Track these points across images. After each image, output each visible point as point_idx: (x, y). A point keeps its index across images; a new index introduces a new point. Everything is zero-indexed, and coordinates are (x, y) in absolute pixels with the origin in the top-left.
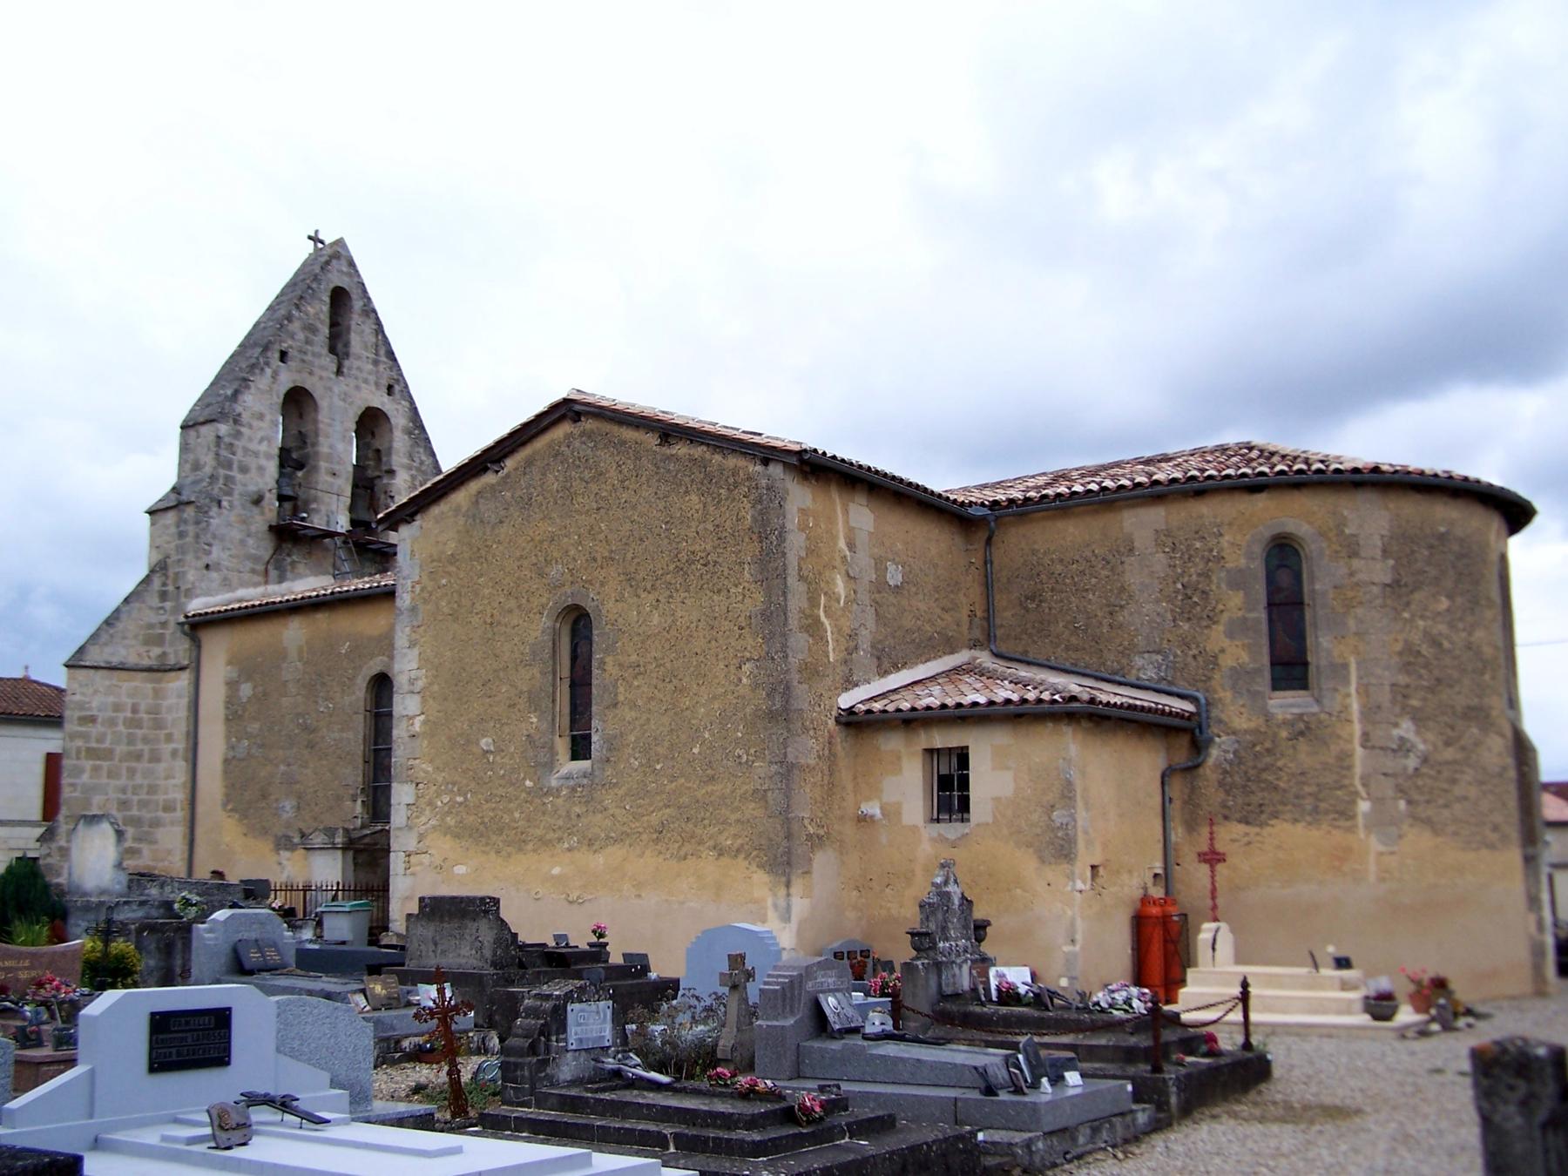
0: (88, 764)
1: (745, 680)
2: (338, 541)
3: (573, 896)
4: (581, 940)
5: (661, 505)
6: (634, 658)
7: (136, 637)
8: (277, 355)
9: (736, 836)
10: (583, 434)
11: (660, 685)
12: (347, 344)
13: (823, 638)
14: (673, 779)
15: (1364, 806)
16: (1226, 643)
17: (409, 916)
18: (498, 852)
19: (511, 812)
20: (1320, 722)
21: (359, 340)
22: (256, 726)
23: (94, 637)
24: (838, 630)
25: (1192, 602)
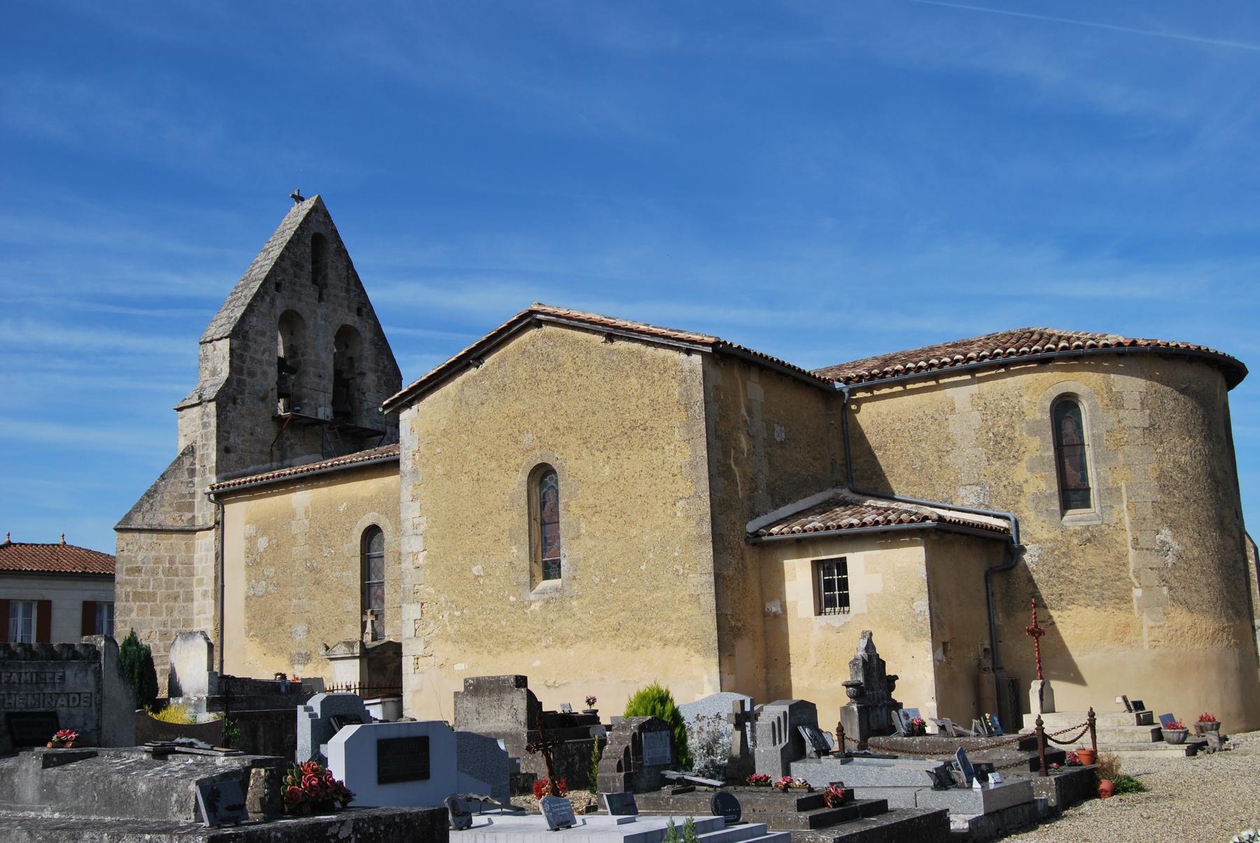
0: (135, 605)
1: (679, 514)
2: (325, 427)
3: (550, 682)
4: (580, 708)
5: (608, 387)
6: (591, 501)
7: (171, 505)
8: (273, 286)
9: (677, 630)
10: (544, 336)
11: (613, 520)
12: (325, 277)
13: (734, 481)
14: (626, 589)
15: (1137, 593)
16: (1029, 475)
17: (456, 694)
18: (489, 652)
19: (499, 621)
20: (1102, 531)
21: (333, 275)
22: (273, 570)
23: (138, 507)
24: (744, 475)
25: (1000, 446)
